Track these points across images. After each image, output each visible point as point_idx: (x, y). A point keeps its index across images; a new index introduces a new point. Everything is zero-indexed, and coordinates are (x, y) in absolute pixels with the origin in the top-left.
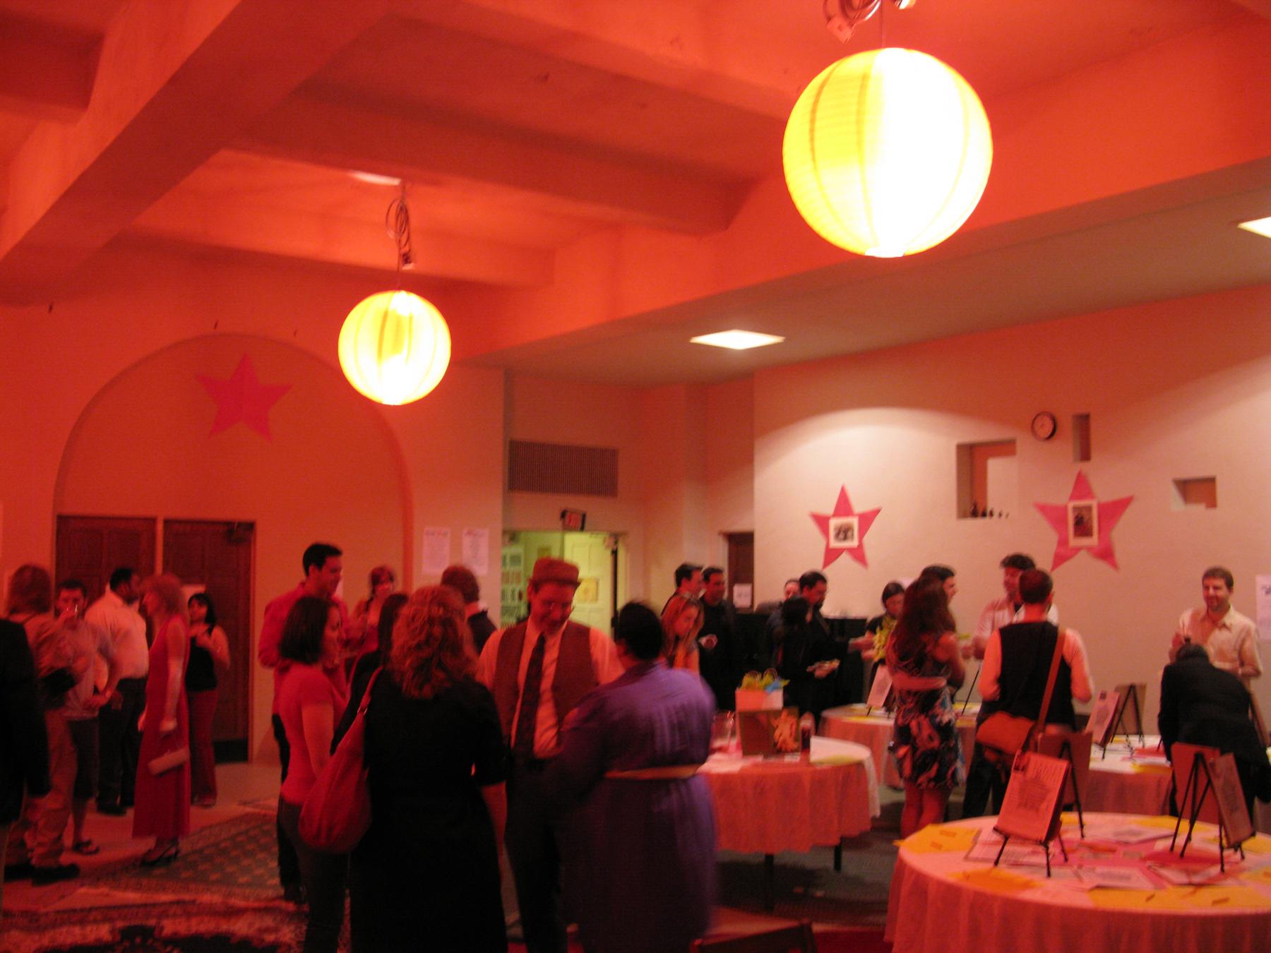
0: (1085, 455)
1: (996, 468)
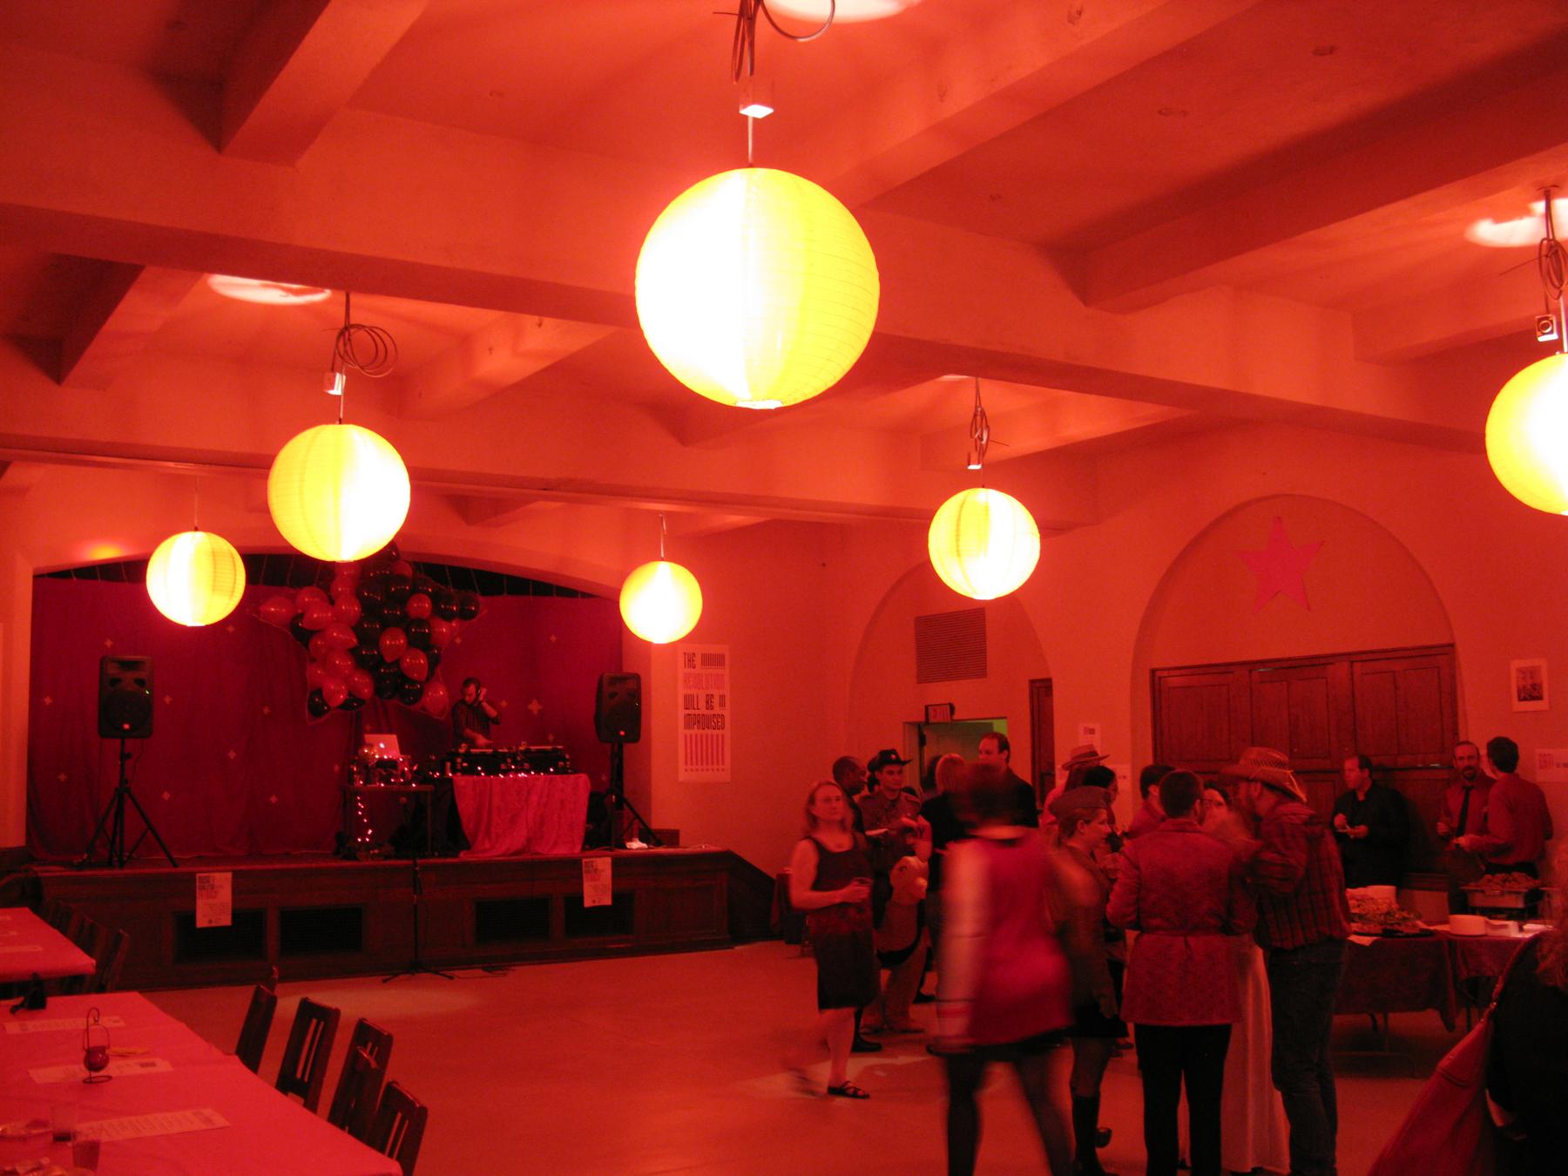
0: (346, 330)
1: (948, 707)
